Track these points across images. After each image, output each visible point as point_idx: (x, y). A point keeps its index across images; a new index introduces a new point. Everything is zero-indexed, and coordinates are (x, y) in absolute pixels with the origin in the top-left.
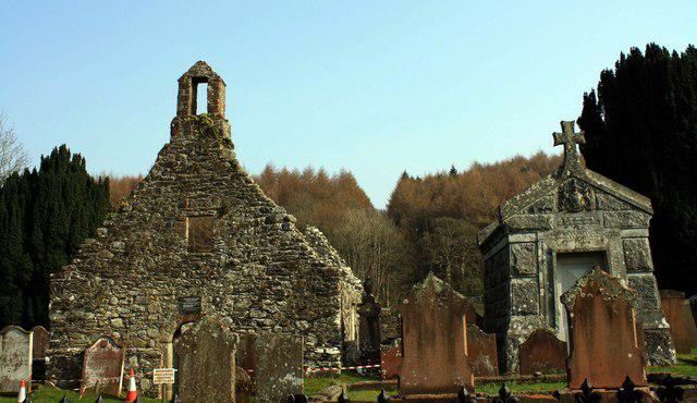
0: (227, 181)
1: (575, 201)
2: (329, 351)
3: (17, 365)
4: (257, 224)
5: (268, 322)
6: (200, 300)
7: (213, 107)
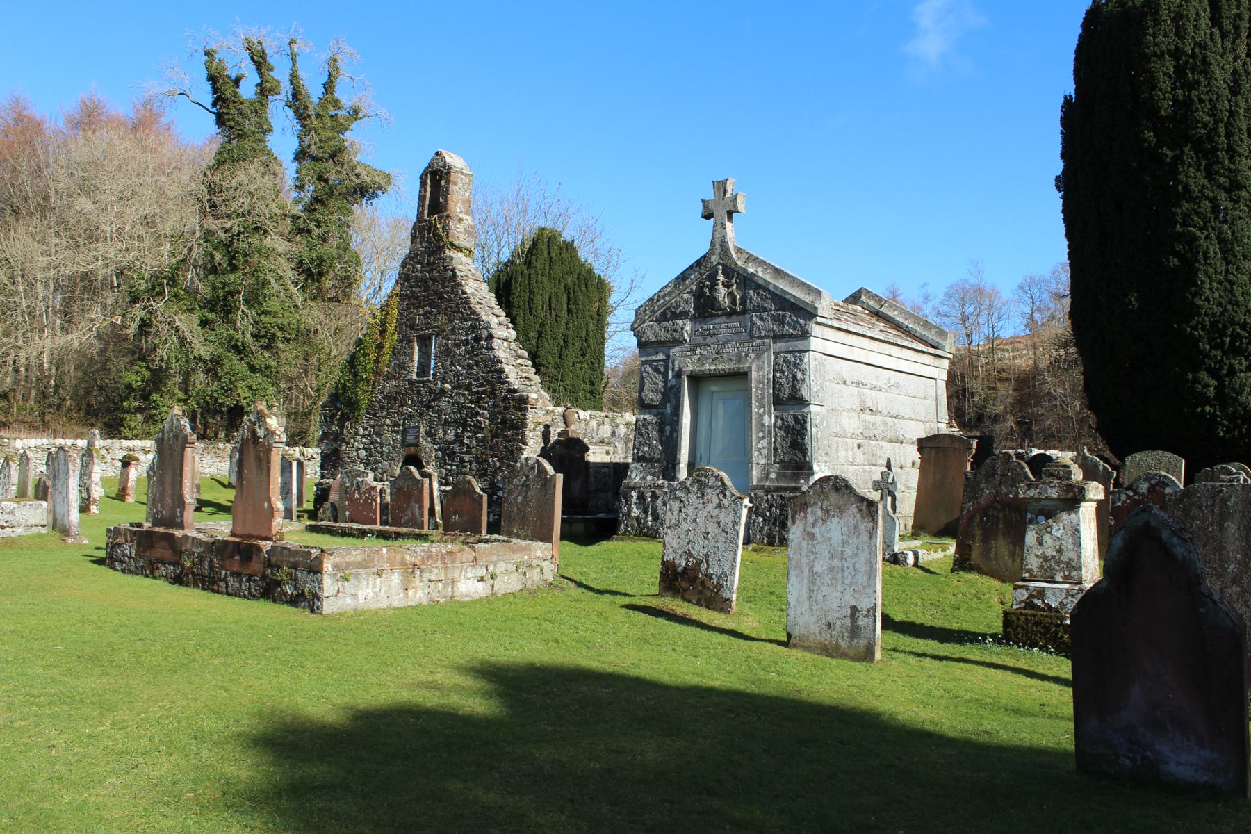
5: (467, 457)
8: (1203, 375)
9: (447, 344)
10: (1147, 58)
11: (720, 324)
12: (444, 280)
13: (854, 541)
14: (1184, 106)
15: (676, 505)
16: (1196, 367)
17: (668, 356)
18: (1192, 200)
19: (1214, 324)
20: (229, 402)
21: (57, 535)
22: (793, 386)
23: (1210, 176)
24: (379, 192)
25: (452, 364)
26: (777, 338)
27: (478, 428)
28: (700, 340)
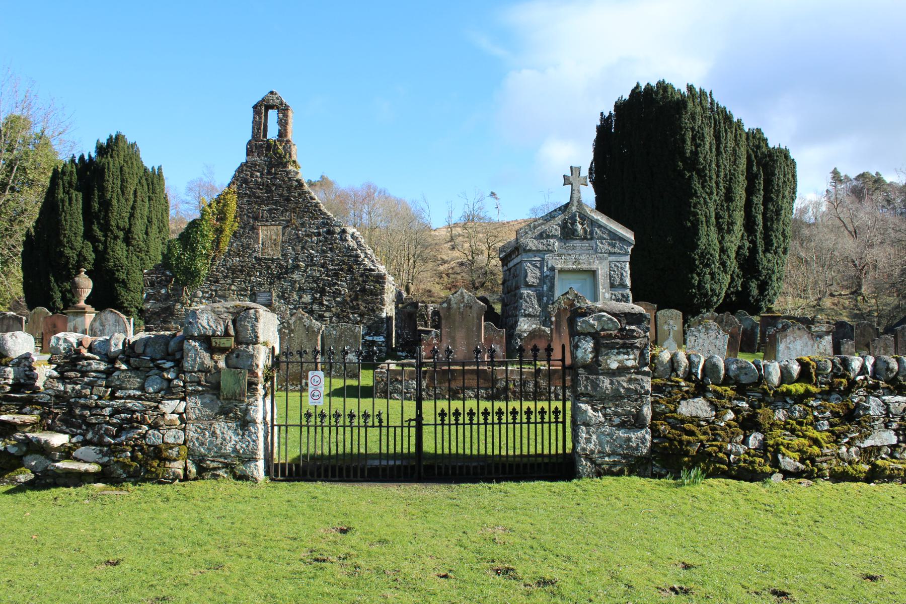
0: (294, 197)
1: (576, 230)
2: (376, 339)
4: (319, 234)
5: (327, 314)
6: (271, 296)
7: (282, 134)
8: (695, 275)
10: (681, 129)
11: (577, 243)
12: (289, 188)
13: (806, 349)
14: (695, 154)
15: (693, 338)
16: (692, 272)
17: (543, 259)
18: (698, 197)
19: (702, 253)
22: (621, 279)
23: (703, 187)
25: (303, 248)
26: (610, 253)
27: (337, 293)
28: (564, 251)
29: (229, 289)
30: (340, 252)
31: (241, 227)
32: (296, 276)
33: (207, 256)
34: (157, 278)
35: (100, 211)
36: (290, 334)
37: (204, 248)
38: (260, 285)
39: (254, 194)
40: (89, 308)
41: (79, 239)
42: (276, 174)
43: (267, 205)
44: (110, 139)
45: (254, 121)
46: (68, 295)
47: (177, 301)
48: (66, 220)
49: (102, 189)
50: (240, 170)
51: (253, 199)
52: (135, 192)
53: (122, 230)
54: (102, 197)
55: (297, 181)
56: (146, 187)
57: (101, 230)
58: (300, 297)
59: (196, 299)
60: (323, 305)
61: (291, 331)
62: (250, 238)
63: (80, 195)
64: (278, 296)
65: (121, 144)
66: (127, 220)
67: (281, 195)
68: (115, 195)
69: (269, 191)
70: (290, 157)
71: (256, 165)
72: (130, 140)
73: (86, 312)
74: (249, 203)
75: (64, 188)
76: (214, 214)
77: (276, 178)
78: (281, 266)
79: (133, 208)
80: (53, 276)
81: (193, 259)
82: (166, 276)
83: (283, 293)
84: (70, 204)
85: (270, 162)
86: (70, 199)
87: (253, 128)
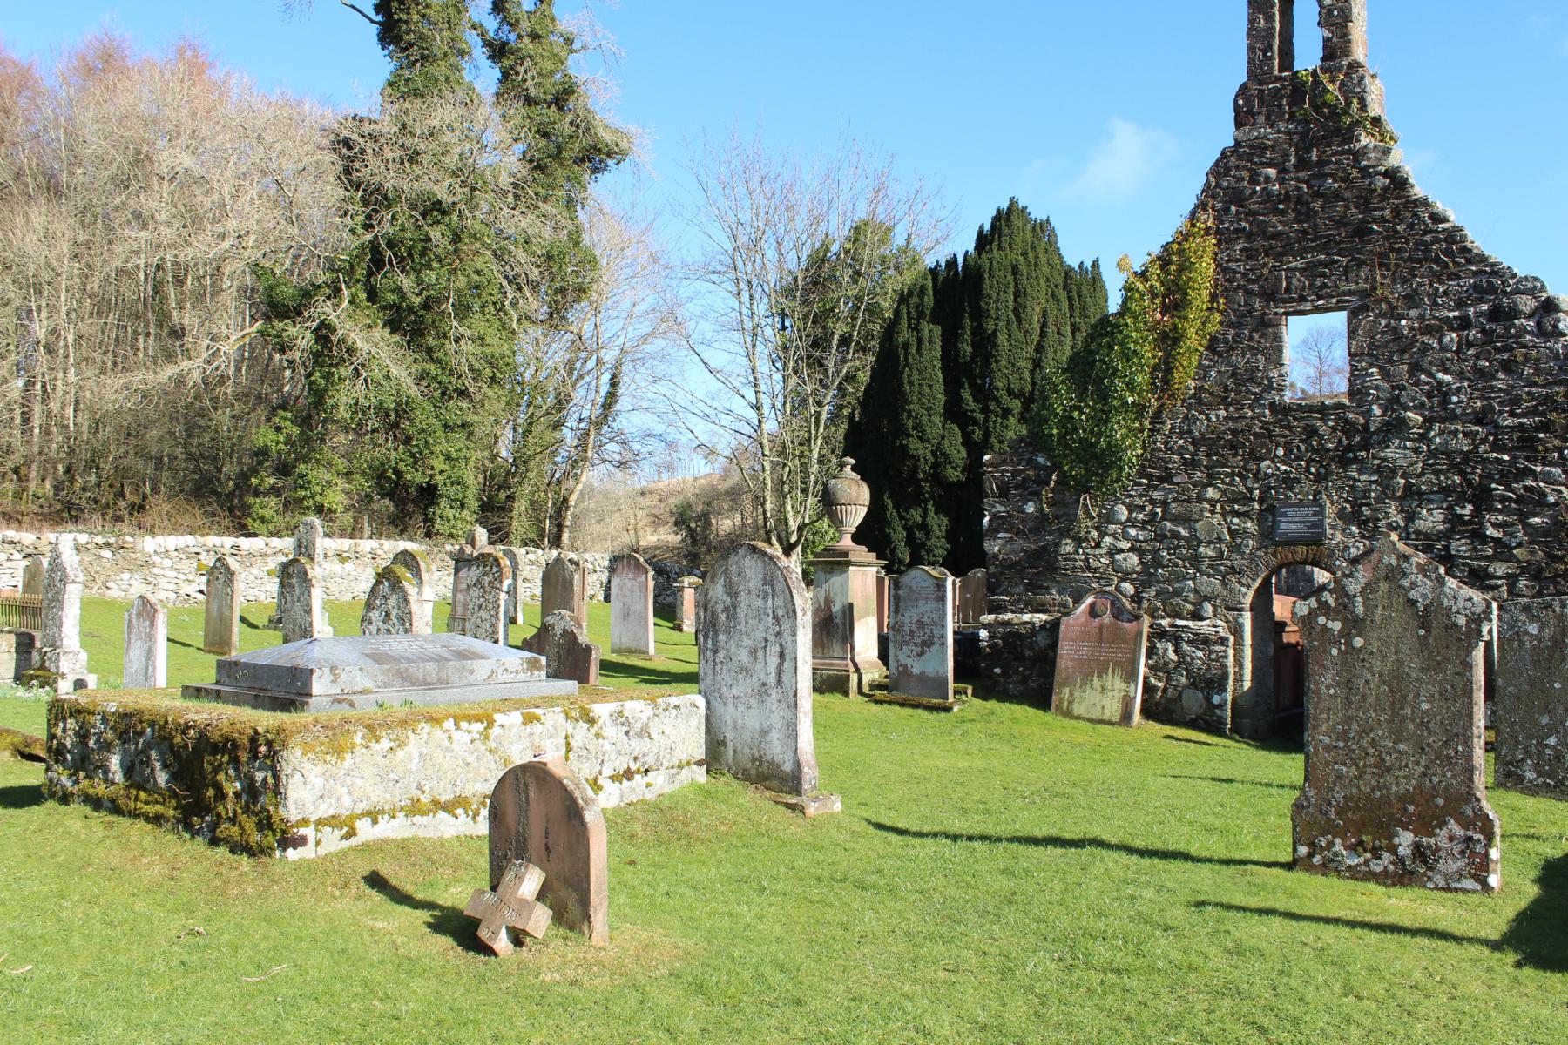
0: (1382, 221)
3: (924, 644)
4: (1464, 323)
5: (1499, 568)
6: (1321, 513)
7: (1336, 49)
9: (1395, 330)
12: (1364, 200)
20: (415, 477)
21: (749, 798)
24: (611, 162)
25: (1415, 368)
29: (1200, 498)
30: (1538, 372)
31: (1231, 325)
32: (1394, 453)
33: (1140, 409)
34: (1015, 473)
35: (973, 356)
36: (1347, 634)
37: (1131, 387)
38: (1288, 482)
39: (1262, 230)
40: (861, 553)
41: (937, 419)
42: (1321, 163)
43: (1301, 254)
44: (997, 219)
45: (1252, 32)
46: (919, 535)
47: (1064, 533)
48: (911, 384)
49: (979, 315)
50: (1220, 168)
51: (1260, 242)
52: (1044, 314)
53: (1017, 396)
54: (978, 331)
55: (1386, 174)
56: (1065, 304)
57: (976, 400)
58: (1410, 517)
59: (1112, 527)
60: (1485, 539)
61: (1354, 625)
62: (1255, 351)
63: (937, 331)
64: (1341, 514)
65: (1017, 222)
66: (1027, 375)
67: (1341, 222)
68: (1002, 324)
69: (1304, 212)
70: (1363, 106)
71: (1264, 148)
72: (1037, 213)
73: (848, 564)
74: (1249, 255)
75: (909, 318)
76: (1154, 296)
77: (1325, 176)
78: (1348, 427)
79: (1040, 349)
80: (890, 497)
81: (1102, 418)
82: (1037, 467)
83: (1357, 506)
84: (919, 350)
85: (1304, 135)
86: (920, 340)
87: (1251, 49)
